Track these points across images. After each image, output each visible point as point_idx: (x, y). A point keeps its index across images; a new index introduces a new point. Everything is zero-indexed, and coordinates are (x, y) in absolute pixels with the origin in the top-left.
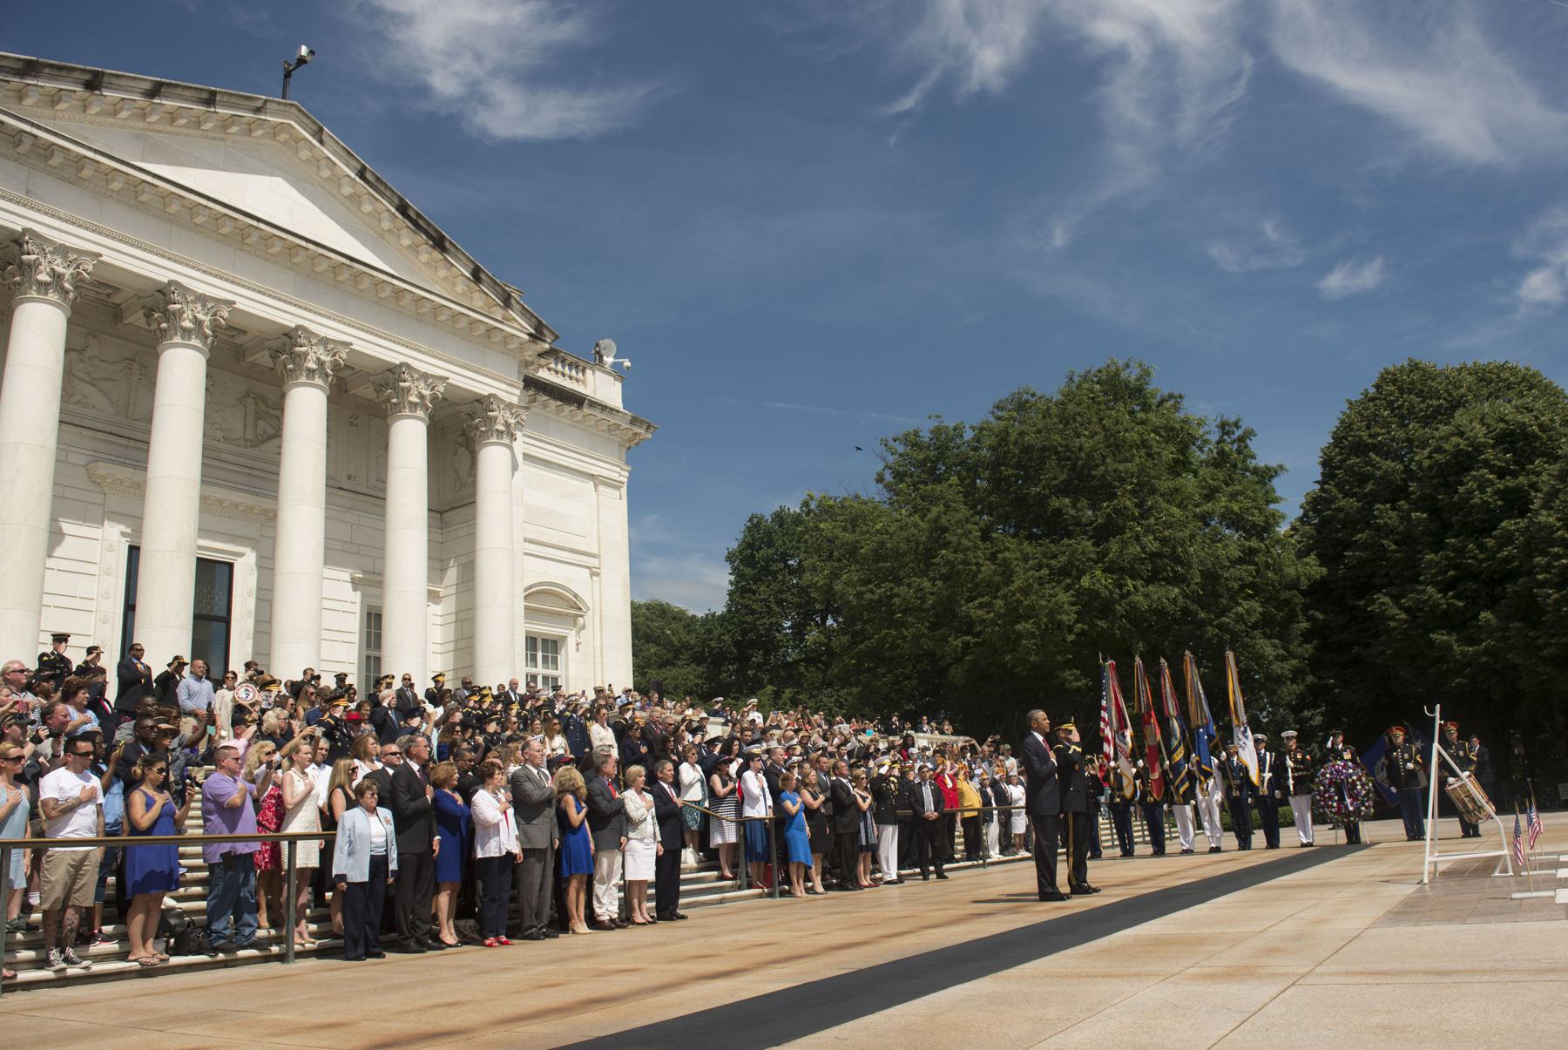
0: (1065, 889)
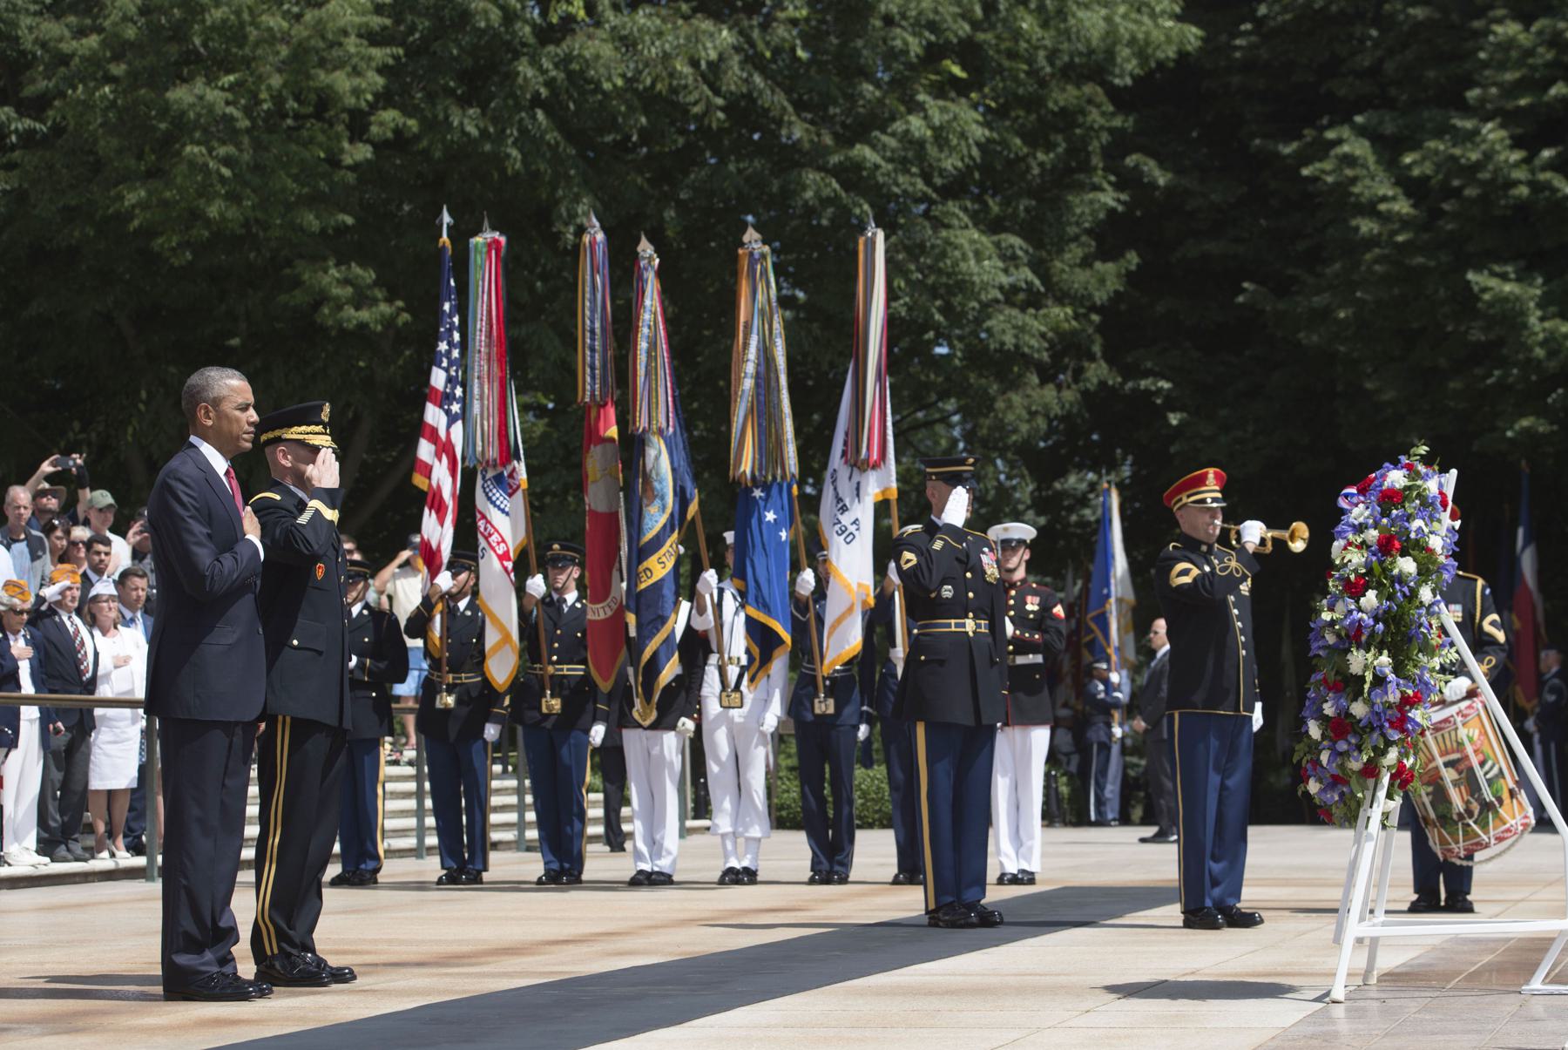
0: (247, 969)
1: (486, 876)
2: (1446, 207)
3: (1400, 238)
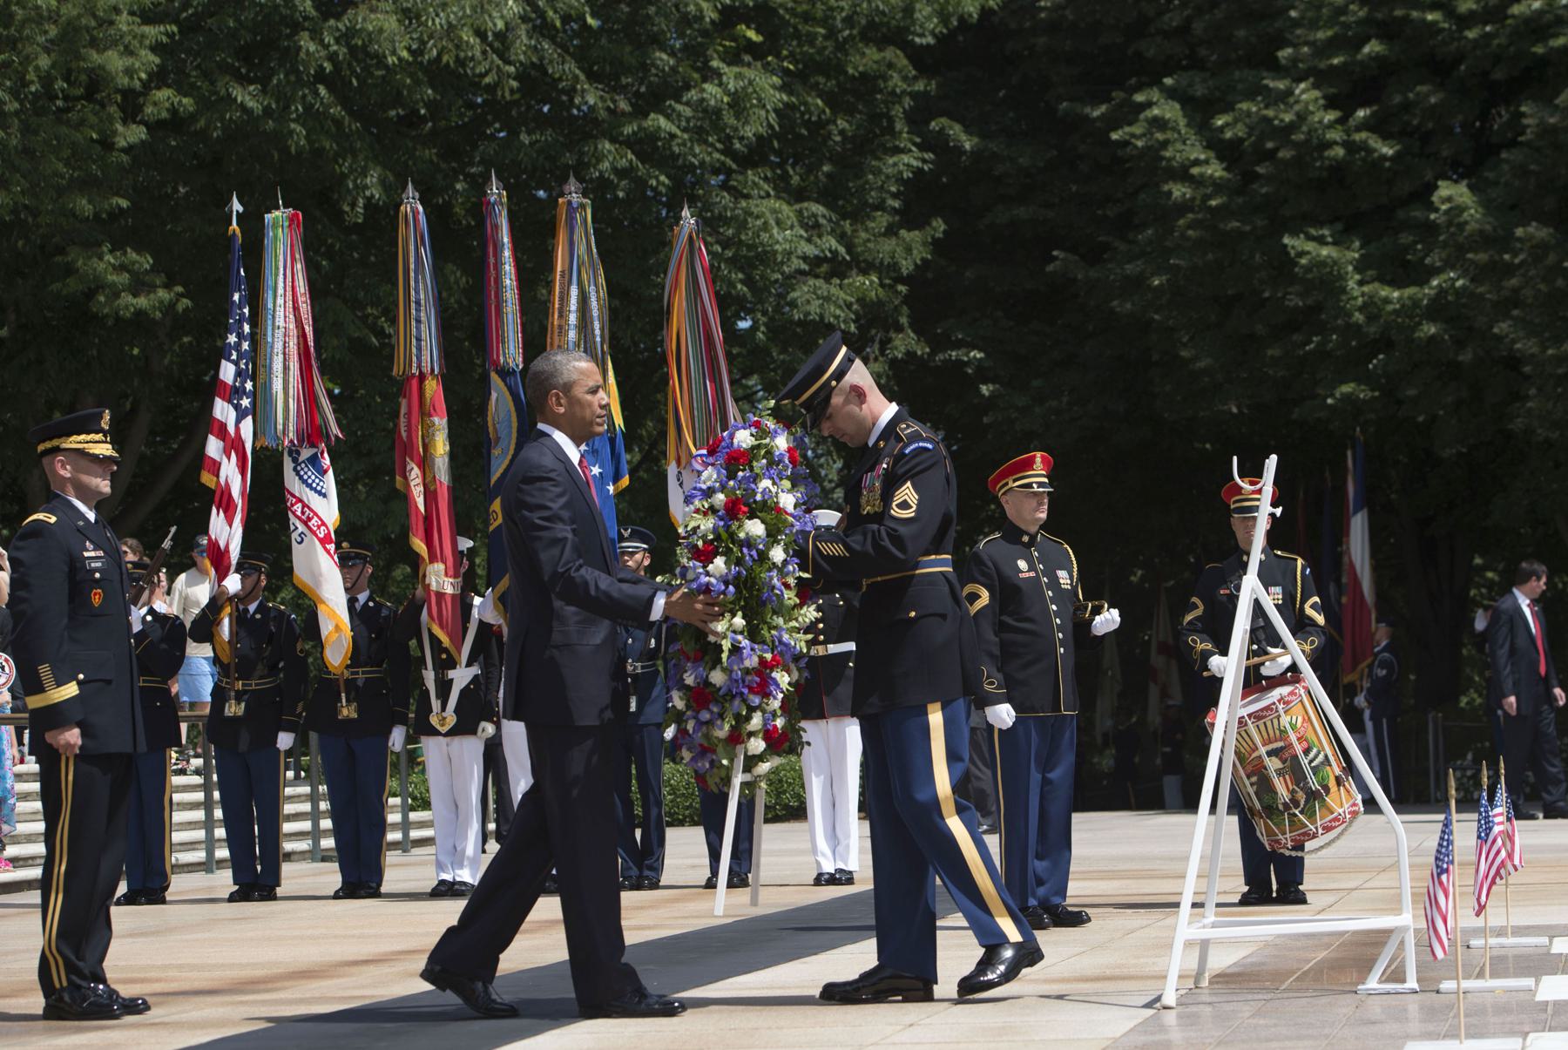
1: (279, 891)
2: (1260, 170)
3: (1213, 203)
